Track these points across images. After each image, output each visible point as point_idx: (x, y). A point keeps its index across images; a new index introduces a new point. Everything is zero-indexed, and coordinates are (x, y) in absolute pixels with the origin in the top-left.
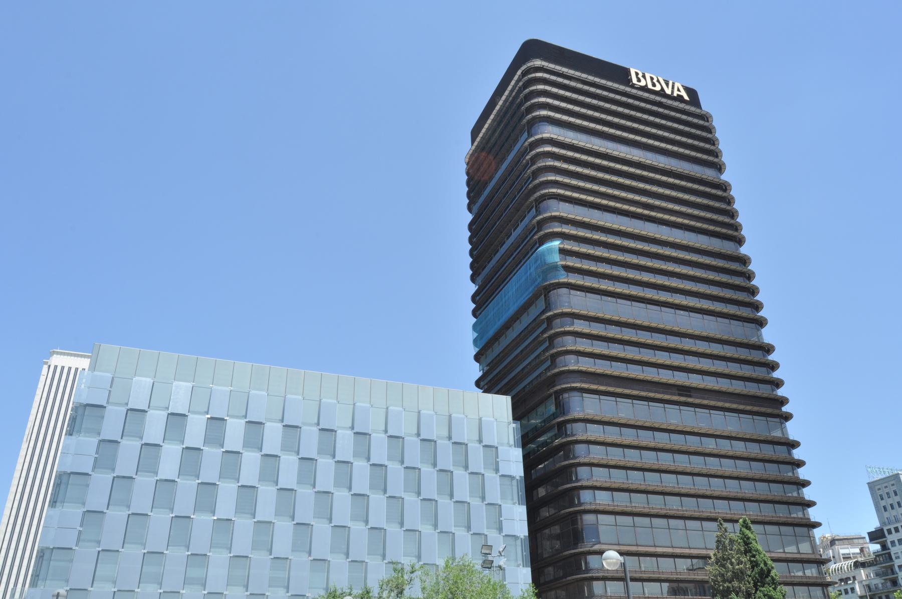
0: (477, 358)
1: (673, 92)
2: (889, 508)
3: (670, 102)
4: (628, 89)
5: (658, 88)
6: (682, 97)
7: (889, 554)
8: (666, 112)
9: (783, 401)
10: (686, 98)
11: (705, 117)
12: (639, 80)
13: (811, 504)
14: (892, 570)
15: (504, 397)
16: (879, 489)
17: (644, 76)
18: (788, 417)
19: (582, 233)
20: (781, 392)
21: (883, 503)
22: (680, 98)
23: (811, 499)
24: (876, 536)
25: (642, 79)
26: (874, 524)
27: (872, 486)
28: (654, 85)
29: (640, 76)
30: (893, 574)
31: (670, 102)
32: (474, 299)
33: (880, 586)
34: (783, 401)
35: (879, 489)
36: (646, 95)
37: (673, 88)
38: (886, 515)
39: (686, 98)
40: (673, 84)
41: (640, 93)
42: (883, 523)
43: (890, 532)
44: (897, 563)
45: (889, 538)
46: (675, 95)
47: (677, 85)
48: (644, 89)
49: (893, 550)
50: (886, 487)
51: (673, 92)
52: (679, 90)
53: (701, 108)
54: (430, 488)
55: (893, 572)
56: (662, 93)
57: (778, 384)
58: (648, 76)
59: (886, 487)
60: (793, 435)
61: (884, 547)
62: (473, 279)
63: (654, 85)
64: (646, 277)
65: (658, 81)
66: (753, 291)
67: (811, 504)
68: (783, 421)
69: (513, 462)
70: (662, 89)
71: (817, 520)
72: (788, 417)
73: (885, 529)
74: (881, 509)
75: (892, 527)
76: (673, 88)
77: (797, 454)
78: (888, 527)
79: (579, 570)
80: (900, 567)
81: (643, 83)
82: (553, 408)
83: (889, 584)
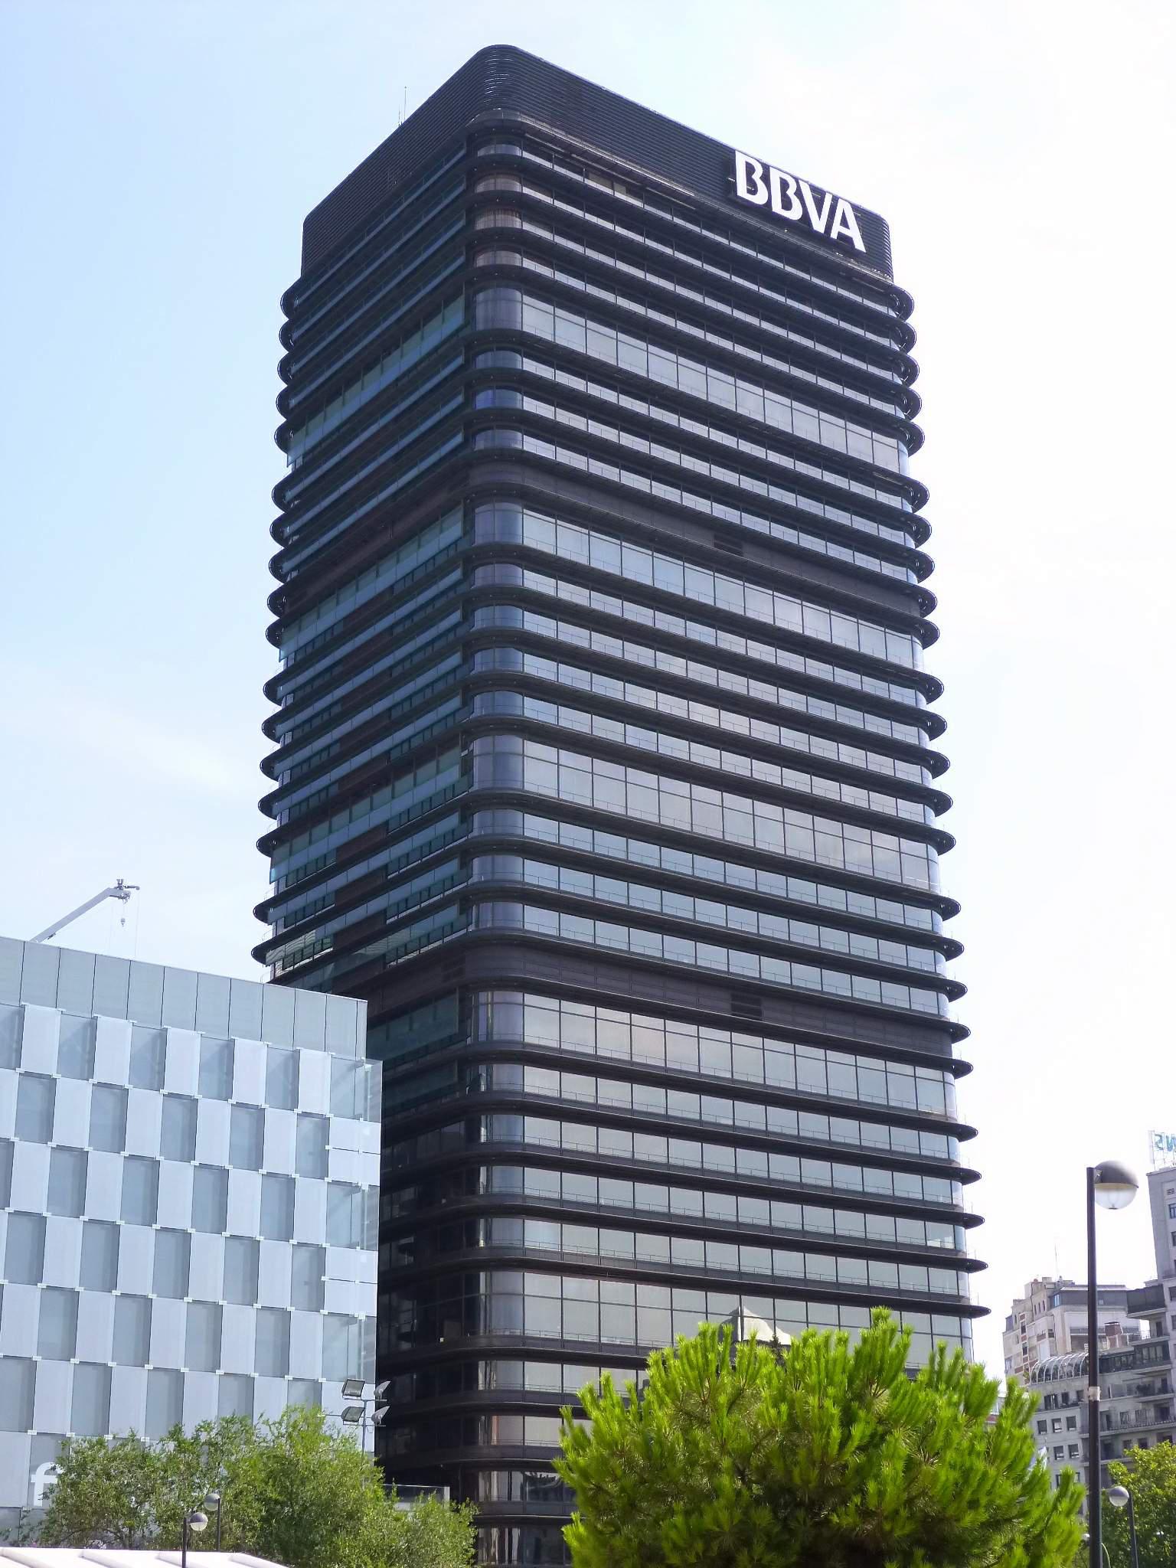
0: (274, 635)
4: (726, 210)
5: (795, 214)
10: (859, 245)
11: (904, 303)
12: (753, 189)
13: (969, 1177)
18: (962, 1069)
19: (750, 1116)
20: (954, 1012)
23: (927, 672)
25: (761, 185)
27: (1090, 1171)
28: (787, 204)
32: (279, 494)
33: (1133, 1416)
34: (959, 1032)
39: (859, 245)
46: (834, 235)
52: (844, 222)
61: (1158, 1328)
62: (283, 439)
63: (787, 204)
65: (799, 193)
66: (922, 531)
67: (969, 1177)
68: (950, 1077)
69: (360, 1152)
70: (806, 216)
71: (976, 1212)
77: (965, 1154)
81: (760, 199)
82: (456, 1079)
83: (1151, 1413)
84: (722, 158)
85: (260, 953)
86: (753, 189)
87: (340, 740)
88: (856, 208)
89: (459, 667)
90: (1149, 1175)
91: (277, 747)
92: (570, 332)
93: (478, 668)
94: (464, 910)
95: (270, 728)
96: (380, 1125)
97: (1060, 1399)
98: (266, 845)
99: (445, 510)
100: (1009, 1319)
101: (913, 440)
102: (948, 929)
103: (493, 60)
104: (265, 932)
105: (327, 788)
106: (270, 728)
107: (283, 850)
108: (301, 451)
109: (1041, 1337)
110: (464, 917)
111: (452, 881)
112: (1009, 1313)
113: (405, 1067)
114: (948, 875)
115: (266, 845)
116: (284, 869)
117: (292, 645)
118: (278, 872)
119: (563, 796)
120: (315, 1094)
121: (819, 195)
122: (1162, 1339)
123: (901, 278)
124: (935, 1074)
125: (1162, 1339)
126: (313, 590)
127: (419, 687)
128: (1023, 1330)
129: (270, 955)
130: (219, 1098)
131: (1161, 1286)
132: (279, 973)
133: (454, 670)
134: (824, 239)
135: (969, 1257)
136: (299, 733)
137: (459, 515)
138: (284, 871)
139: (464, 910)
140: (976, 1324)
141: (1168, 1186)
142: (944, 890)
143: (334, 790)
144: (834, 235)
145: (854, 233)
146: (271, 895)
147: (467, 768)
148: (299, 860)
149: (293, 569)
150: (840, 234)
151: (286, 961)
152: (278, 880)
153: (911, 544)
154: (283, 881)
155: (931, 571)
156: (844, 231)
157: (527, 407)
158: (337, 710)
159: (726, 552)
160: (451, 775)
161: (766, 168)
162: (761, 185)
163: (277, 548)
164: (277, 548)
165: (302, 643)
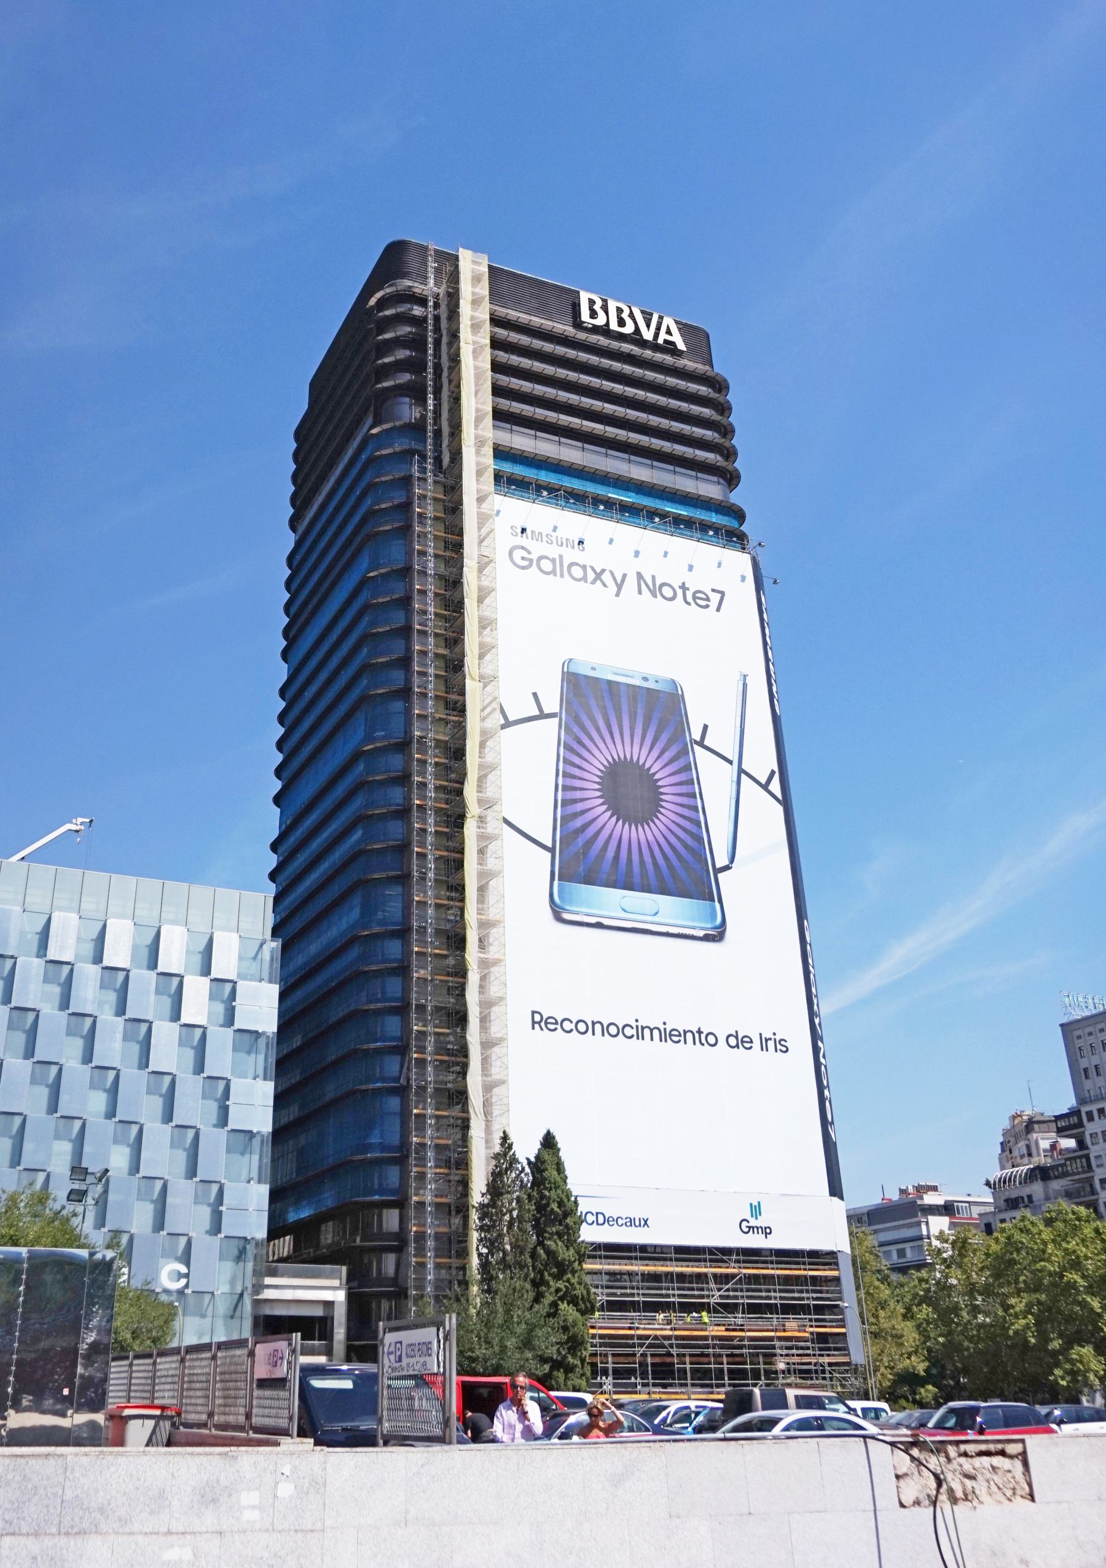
1: (656, 335)
3: (648, 353)
5: (629, 329)
6: (673, 343)
7: (1087, 1157)
8: (638, 372)
10: (681, 346)
11: (719, 385)
12: (593, 314)
14: (1092, 1186)
15: (129, 959)
16: (1079, 1037)
17: (605, 308)
21: (1084, 1063)
22: (669, 348)
24: (1069, 1123)
25: (601, 313)
26: (1064, 1101)
27: (1067, 1028)
28: (621, 323)
29: (597, 307)
30: (1093, 1194)
31: (648, 353)
35: (1079, 1037)
36: (603, 341)
37: (658, 328)
40: (661, 318)
41: (594, 338)
42: (1082, 1100)
43: (1090, 1117)
44: (1099, 1174)
45: (1090, 1128)
46: (660, 341)
47: (668, 321)
48: (605, 331)
49: (1094, 1151)
50: (1090, 1034)
51: (656, 335)
52: (669, 332)
53: (712, 366)
54: (112, 1046)
55: (1093, 1192)
56: (635, 338)
58: (612, 305)
59: (1090, 1034)
61: (1081, 1144)
63: (621, 323)
69: (262, 1007)
70: (637, 330)
73: (1084, 1109)
74: (1079, 1074)
76: (658, 328)
80: (1102, 1181)
81: (601, 321)
90: (1062, 1025)
96: (277, 986)
97: (1026, 1200)
100: (1002, 1144)
101: (731, 479)
109: (1022, 1157)
112: (1001, 1139)
120: (225, 964)
122: (1085, 1152)
125: (464, 1115)
128: (1011, 1152)
130: (202, 975)
131: (1079, 1111)
134: (655, 347)
141: (1076, 1033)
144: (660, 341)
150: (666, 341)
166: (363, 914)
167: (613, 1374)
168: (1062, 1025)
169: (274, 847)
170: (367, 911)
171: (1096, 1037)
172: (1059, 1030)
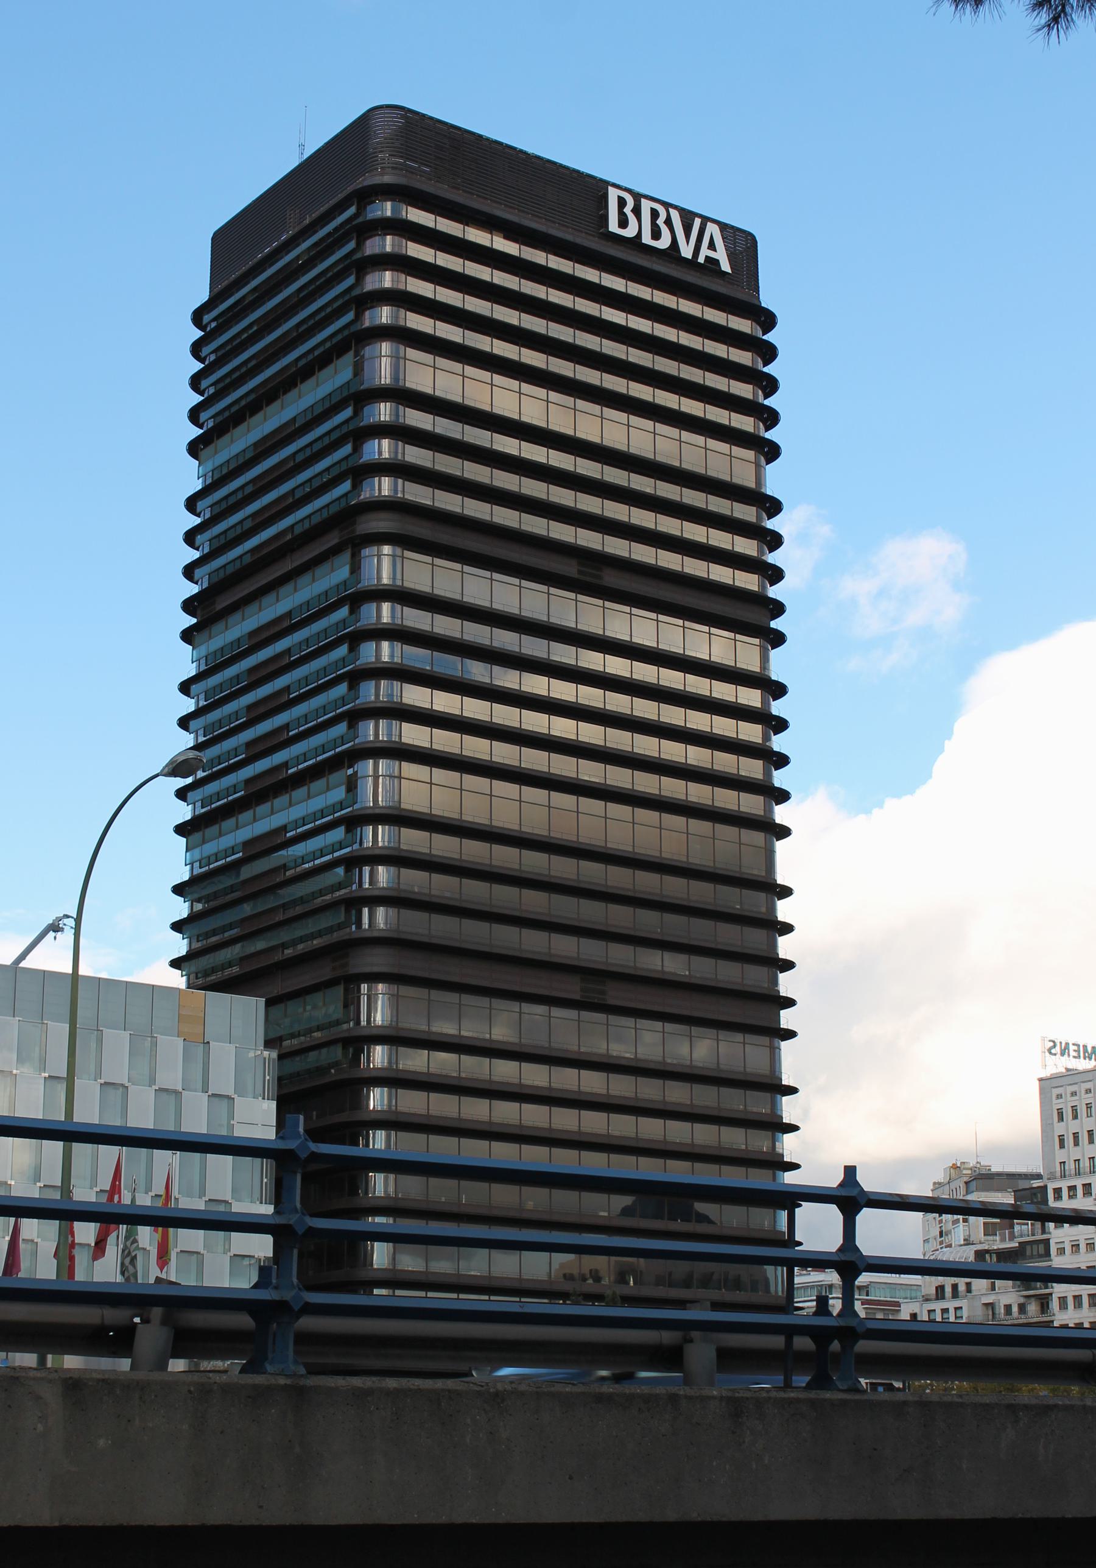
2: (1069, 1141)
6: (716, 262)
9: (777, 609)
10: (726, 267)
12: (623, 223)
17: (637, 211)
18: (778, 639)
20: (774, 592)
21: (1059, 1129)
25: (632, 218)
28: (656, 234)
34: (777, 609)
38: (1060, 1155)
39: (726, 267)
48: (635, 242)
50: (1074, 1094)
52: (712, 246)
57: (780, 725)
59: (1074, 1094)
60: (772, 488)
63: (656, 234)
64: (643, 518)
65: (668, 222)
66: (769, 353)
72: (778, 639)
73: (1051, 1186)
75: (1079, 1182)
78: (1057, 1185)
79: (353, 1191)
81: (630, 232)
82: (342, 919)
84: (593, 190)
85: (184, 723)
86: (623, 223)
87: (253, 481)
88: (723, 227)
89: (350, 455)
91: (197, 521)
92: (426, 374)
93: (367, 324)
94: (352, 725)
95: (195, 382)
98: (187, 636)
99: (335, 551)
102: (778, 708)
103: (382, 131)
104: (188, 705)
105: (241, 557)
106: (194, 416)
107: (197, 836)
108: (210, 465)
110: (350, 835)
111: (343, 701)
113: (295, 1041)
114: (776, 480)
115: (187, 636)
116: (197, 853)
117: (203, 650)
118: (192, 856)
119: (436, 592)
120: (223, 1081)
121: (688, 217)
123: (767, 299)
124: (750, 454)
126: (222, 602)
127: (317, 436)
129: (193, 724)
132: (201, 739)
133: (346, 458)
134: (692, 263)
135: (769, 492)
136: (217, 510)
137: (346, 556)
138: (197, 856)
139: (352, 725)
140: (780, 846)
142: (770, 490)
143: (247, 559)
145: (721, 255)
146: (193, 673)
147: (352, 785)
148: (210, 848)
149: (212, 353)
150: (708, 259)
151: (207, 694)
152: (192, 864)
153: (759, 333)
154: (203, 661)
155: (788, 763)
156: (711, 254)
157: (411, 253)
158: (249, 489)
159: (592, 576)
160: (339, 794)
161: (637, 197)
162: (632, 218)
163: (198, 334)
164: (198, 334)
165: (217, 463)
166: (358, 209)
167: (296, 1343)
168: (1040, 1080)
169: (191, 504)
170: (356, 413)
171: (1066, 1102)
172: (1036, 1087)
